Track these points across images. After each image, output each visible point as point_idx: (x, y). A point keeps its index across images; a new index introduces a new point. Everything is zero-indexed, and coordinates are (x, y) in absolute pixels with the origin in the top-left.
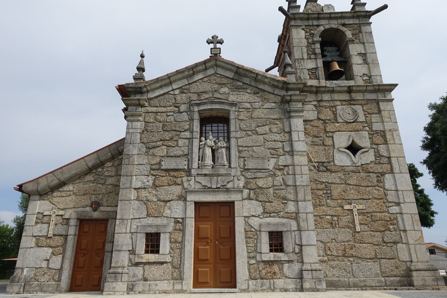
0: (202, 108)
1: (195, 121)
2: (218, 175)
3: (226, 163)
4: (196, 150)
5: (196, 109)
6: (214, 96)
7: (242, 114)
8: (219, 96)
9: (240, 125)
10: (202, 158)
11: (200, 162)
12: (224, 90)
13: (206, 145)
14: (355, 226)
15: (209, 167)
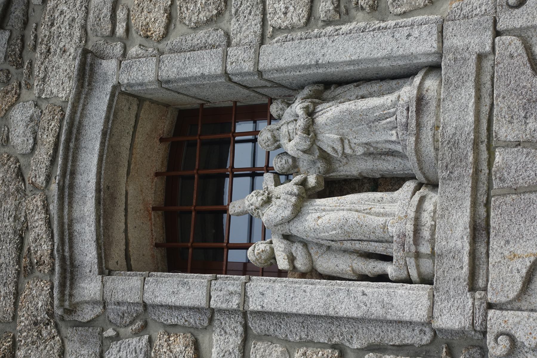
0: (88, 252)
1: (149, 298)
2: (485, 140)
3: (407, 92)
4: (310, 297)
5: (90, 287)
6: (41, 180)
7: (137, 21)
8: (43, 154)
9: (197, 27)
10: (373, 260)
11: (390, 269)
12: (20, 130)
13: (298, 228)
14: (515, 310)
15: (428, 206)
